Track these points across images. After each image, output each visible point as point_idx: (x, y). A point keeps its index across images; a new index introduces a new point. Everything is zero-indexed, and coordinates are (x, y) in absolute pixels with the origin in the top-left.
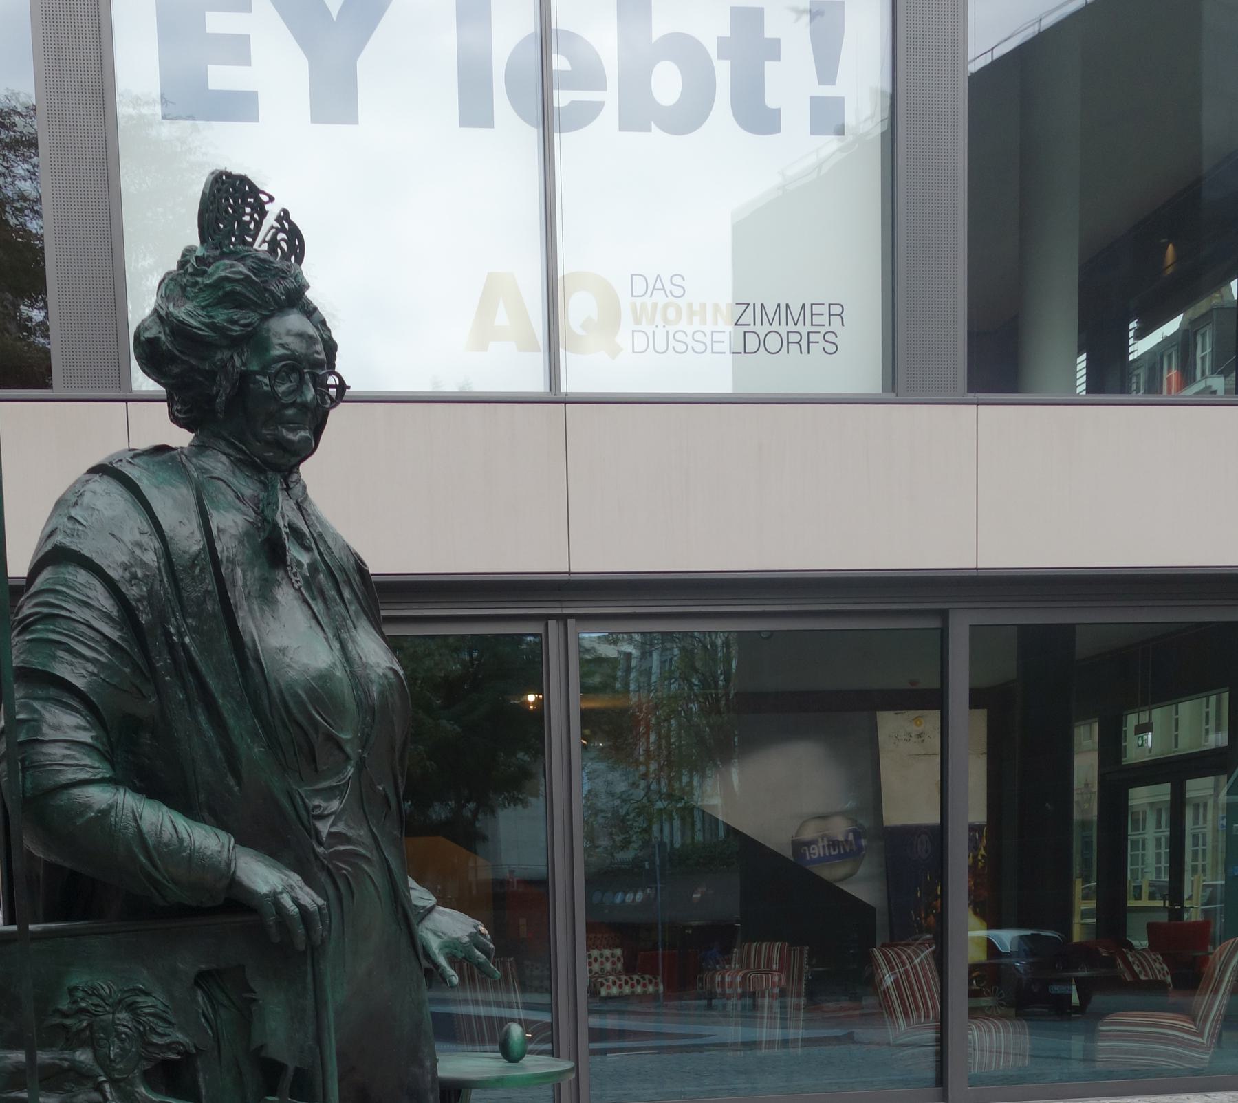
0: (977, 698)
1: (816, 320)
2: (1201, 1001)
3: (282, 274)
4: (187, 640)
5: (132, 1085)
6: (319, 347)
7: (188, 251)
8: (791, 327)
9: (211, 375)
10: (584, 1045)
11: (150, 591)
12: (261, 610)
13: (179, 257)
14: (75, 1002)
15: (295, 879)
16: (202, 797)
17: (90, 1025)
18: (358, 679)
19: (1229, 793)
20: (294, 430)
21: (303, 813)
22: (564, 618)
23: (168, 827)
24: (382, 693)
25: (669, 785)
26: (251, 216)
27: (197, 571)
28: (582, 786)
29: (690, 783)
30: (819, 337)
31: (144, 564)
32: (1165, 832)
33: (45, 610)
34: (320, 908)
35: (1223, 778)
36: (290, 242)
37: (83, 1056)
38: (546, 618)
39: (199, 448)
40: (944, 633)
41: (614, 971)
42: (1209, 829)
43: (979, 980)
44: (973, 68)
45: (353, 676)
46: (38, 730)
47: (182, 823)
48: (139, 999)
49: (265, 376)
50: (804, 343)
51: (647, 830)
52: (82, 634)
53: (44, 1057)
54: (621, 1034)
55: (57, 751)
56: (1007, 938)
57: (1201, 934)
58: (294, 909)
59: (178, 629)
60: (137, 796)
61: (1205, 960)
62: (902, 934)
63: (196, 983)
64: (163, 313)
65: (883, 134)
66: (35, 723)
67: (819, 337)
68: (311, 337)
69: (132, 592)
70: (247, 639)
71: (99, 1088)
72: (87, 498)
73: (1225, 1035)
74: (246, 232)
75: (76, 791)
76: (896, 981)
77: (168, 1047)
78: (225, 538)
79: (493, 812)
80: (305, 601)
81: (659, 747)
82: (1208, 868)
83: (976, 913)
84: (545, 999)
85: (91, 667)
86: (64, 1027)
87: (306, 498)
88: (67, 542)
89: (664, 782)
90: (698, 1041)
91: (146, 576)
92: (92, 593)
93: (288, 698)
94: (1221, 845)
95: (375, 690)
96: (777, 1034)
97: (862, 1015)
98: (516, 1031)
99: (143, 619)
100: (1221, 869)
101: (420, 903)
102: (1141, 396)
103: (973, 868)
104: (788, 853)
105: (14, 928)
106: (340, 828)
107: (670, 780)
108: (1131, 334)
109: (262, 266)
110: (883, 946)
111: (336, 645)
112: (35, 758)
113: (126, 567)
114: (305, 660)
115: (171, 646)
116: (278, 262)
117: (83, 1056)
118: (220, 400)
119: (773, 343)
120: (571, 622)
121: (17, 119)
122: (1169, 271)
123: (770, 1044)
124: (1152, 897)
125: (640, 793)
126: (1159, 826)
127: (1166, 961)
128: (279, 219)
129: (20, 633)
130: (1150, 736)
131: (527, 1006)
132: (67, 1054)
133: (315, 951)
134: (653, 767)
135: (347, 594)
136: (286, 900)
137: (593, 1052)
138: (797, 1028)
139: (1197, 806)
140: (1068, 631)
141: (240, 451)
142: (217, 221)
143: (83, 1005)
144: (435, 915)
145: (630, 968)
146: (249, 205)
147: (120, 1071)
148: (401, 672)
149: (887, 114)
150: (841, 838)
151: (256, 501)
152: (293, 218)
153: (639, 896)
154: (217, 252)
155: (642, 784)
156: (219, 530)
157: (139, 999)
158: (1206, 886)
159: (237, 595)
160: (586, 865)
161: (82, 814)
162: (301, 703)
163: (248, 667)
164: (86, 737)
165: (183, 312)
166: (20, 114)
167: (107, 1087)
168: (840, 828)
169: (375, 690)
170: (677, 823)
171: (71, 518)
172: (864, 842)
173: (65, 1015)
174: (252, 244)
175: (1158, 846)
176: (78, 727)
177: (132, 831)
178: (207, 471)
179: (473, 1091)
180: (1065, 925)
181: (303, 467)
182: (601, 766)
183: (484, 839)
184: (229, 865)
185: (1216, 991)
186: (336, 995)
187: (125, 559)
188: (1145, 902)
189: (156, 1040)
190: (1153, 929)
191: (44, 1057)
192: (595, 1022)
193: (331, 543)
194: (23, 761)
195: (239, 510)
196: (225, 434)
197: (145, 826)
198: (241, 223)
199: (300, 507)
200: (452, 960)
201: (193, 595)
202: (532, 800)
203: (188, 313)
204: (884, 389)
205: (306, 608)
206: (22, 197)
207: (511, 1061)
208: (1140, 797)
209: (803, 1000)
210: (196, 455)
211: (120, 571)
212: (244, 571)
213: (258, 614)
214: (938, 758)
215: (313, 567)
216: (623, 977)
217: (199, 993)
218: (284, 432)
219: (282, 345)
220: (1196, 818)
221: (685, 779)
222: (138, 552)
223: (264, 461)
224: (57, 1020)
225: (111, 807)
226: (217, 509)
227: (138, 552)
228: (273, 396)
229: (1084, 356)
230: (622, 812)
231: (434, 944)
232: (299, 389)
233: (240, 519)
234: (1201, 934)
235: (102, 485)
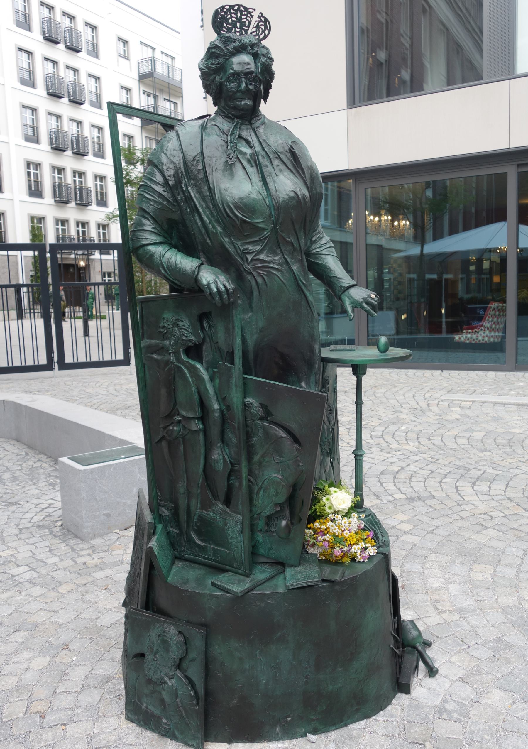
26: (231, 18)
58: (215, 290)
136: (213, 287)
181: (264, 108)
223: (233, 115)
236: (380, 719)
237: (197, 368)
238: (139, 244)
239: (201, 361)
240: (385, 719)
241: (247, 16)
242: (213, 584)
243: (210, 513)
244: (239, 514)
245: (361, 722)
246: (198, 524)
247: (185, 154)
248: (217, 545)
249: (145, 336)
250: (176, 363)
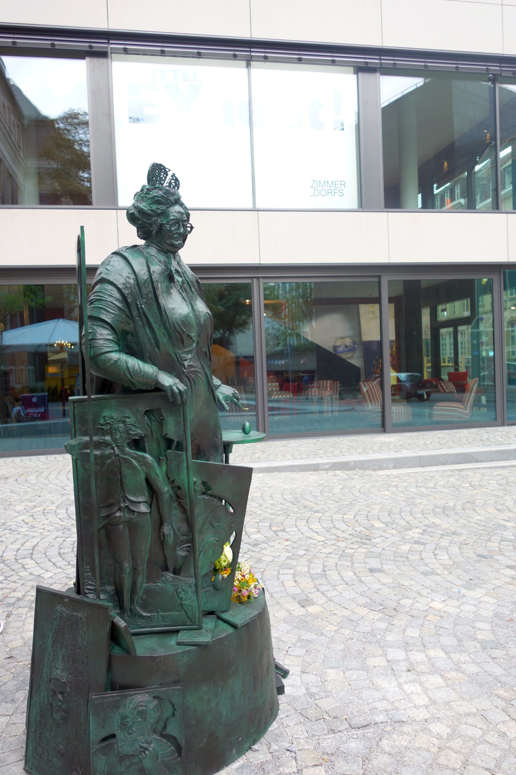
0: (391, 300)
1: (337, 186)
2: (466, 395)
3: (173, 194)
4: (143, 306)
5: (124, 447)
6: (185, 216)
7: (144, 187)
8: (329, 188)
9: (151, 225)
10: (267, 413)
11: (131, 291)
12: (167, 296)
13: (141, 188)
14: (105, 421)
15: (177, 380)
16: (147, 355)
17: (110, 428)
18: (197, 316)
19: (471, 329)
20: (177, 241)
21: (180, 359)
22: (258, 278)
23: (137, 366)
24: (204, 320)
25: (292, 325)
27: (146, 285)
28: (265, 326)
29: (299, 324)
30: (337, 191)
31: (129, 283)
32: (452, 341)
33: (98, 298)
34: (185, 390)
35: (470, 326)
36: (175, 183)
37: (108, 438)
38: (253, 278)
39: (147, 246)
40: (379, 283)
41: (276, 390)
42: (466, 339)
43: (395, 390)
44: (383, 105)
45: (195, 315)
46: (95, 335)
47: (141, 363)
48: (126, 420)
49: (168, 225)
50: (333, 193)
51: (285, 340)
52: (110, 305)
53: (95, 438)
54: (279, 409)
55: (101, 342)
56: (403, 376)
57: (465, 375)
58: (177, 391)
59: (140, 303)
60: (127, 356)
61: (466, 384)
62: (369, 377)
63: (145, 414)
64: (136, 205)
65: (356, 125)
66: (94, 333)
67: (337, 191)
68: (182, 213)
69: (126, 292)
70: (162, 305)
71: (113, 448)
72: (112, 263)
73: (474, 408)
74: (161, 181)
75: (107, 354)
76: (367, 391)
77: (136, 435)
78: (155, 274)
79: (234, 335)
80: (180, 293)
81: (289, 313)
82: (467, 353)
83: (393, 368)
84: (253, 396)
85: (112, 316)
86: (102, 428)
87: (180, 260)
88: (105, 276)
89: (291, 324)
90: (304, 411)
91: (130, 287)
92: (113, 293)
93: (175, 324)
94: (470, 346)
95: (202, 319)
96: (330, 409)
97: (357, 402)
98: (247, 424)
99: (129, 300)
100: (470, 353)
101: (216, 384)
102: (439, 210)
103: (391, 354)
104: (331, 350)
105: (86, 397)
106: (191, 363)
107: (293, 323)
108: (435, 188)
109: (167, 192)
110: (364, 381)
111: (190, 306)
112: (94, 344)
113: (124, 284)
114: (180, 312)
115: (138, 309)
116: (172, 191)
117: (108, 438)
118: (154, 232)
119: (323, 193)
120: (261, 279)
121: (80, 116)
122: (446, 170)
123: (328, 412)
124: (449, 362)
125: (283, 328)
126: (450, 339)
127: (454, 385)
128: (172, 176)
129: (90, 305)
130: (446, 313)
131: (247, 399)
132: (102, 438)
133: (183, 403)
134: (287, 320)
135: (193, 289)
136: (175, 388)
137: (269, 415)
138: (336, 406)
139: (462, 334)
140: (419, 281)
141: (160, 247)
142: (153, 177)
143: (108, 422)
144: (221, 388)
145: (281, 389)
146: (163, 172)
147: (120, 443)
148: (210, 313)
149: (357, 118)
150: (349, 345)
151: (165, 262)
152: (176, 176)
153: (283, 362)
154: (153, 187)
155: (284, 325)
156: (153, 272)
157: (126, 420)
158: (466, 359)
159: (159, 292)
160: (266, 352)
161: (109, 362)
162: (179, 325)
163: (162, 314)
164: (111, 337)
165: (142, 205)
166: (81, 115)
167: (115, 448)
168: (348, 342)
169: (202, 319)
170: (295, 337)
171: (106, 269)
172: (356, 346)
173: (102, 425)
174: (163, 184)
175: (450, 345)
176: (108, 334)
177: (125, 367)
178: (149, 253)
179: (234, 445)
180: (421, 371)
181: (179, 251)
182: (270, 320)
183: (232, 344)
184: (156, 377)
185: (471, 392)
186: (190, 416)
187: (124, 282)
188: (447, 364)
189: (132, 433)
190: (449, 374)
191: (95, 438)
192: (270, 405)
193: (188, 274)
194: (90, 345)
195: (159, 265)
196: (155, 242)
197: (129, 365)
198: (160, 178)
199: (178, 263)
200: (226, 400)
201: (145, 292)
202: (246, 331)
203: (144, 206)
204: (359, 207)
205: (180, 295)
206: (81, 140)
207: (246, 434)
208: (443, 331)
209: (338, 396)
210: (146, 248)
211: (122, 286)
212: (161, 284)
213: (166, 298)
214: (379, 319)
215: (183, 282)
216: (279, 392)
217: (146, 417)
218: (174, 241)
219: (173, 216)
220: (462, 337)
221: (297, 323)
222: (128, 279)
223: (168, 250)
224: (100, 426)
225: (119, 359)
226: (153, 265)
227: (128, 279)
228: (170, 231)
229: (420, 195)
230: (277, 334)
231: (221, 397)
232: (179, 229)
233: (160, 268)
234: (465, 375)
235: (116, 258)
236: (282, 716)
237: (146, 457)
238: (99, 352)
239: (145, 452)
240: (286, 715)
241: (164, 174)
242: (179, 644)
243: (159, 584)
244: (191, 577)
245: (273, 724)
246: (145, 597)
247: (139, 278)
248: (165, 611)
249: (77, 434)
250: (121, 456)
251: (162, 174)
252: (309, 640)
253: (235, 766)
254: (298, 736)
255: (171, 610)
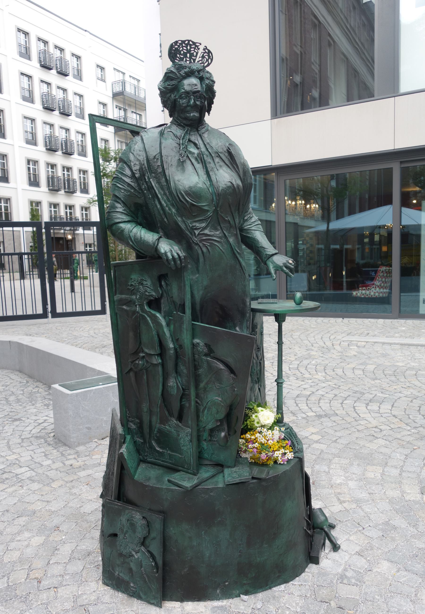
58: (170, 257)
59: (148, 177)
128: (204, 49)
136: (169, 255)
177: (128, 235)
223: (184, 124)
236: (296, 583)
237: (157, 316)
238: (113, 222)
240: (300, 583)
242: (169, 481)
243: (167, 427)
244: (189, 427)
247: (148, 154)
249: (117, 292)
250: (141, 313)
251: (193, 49)
252: (396, 526)
253: (216, 603)
254: (290, 607)
255: (176, 452)
